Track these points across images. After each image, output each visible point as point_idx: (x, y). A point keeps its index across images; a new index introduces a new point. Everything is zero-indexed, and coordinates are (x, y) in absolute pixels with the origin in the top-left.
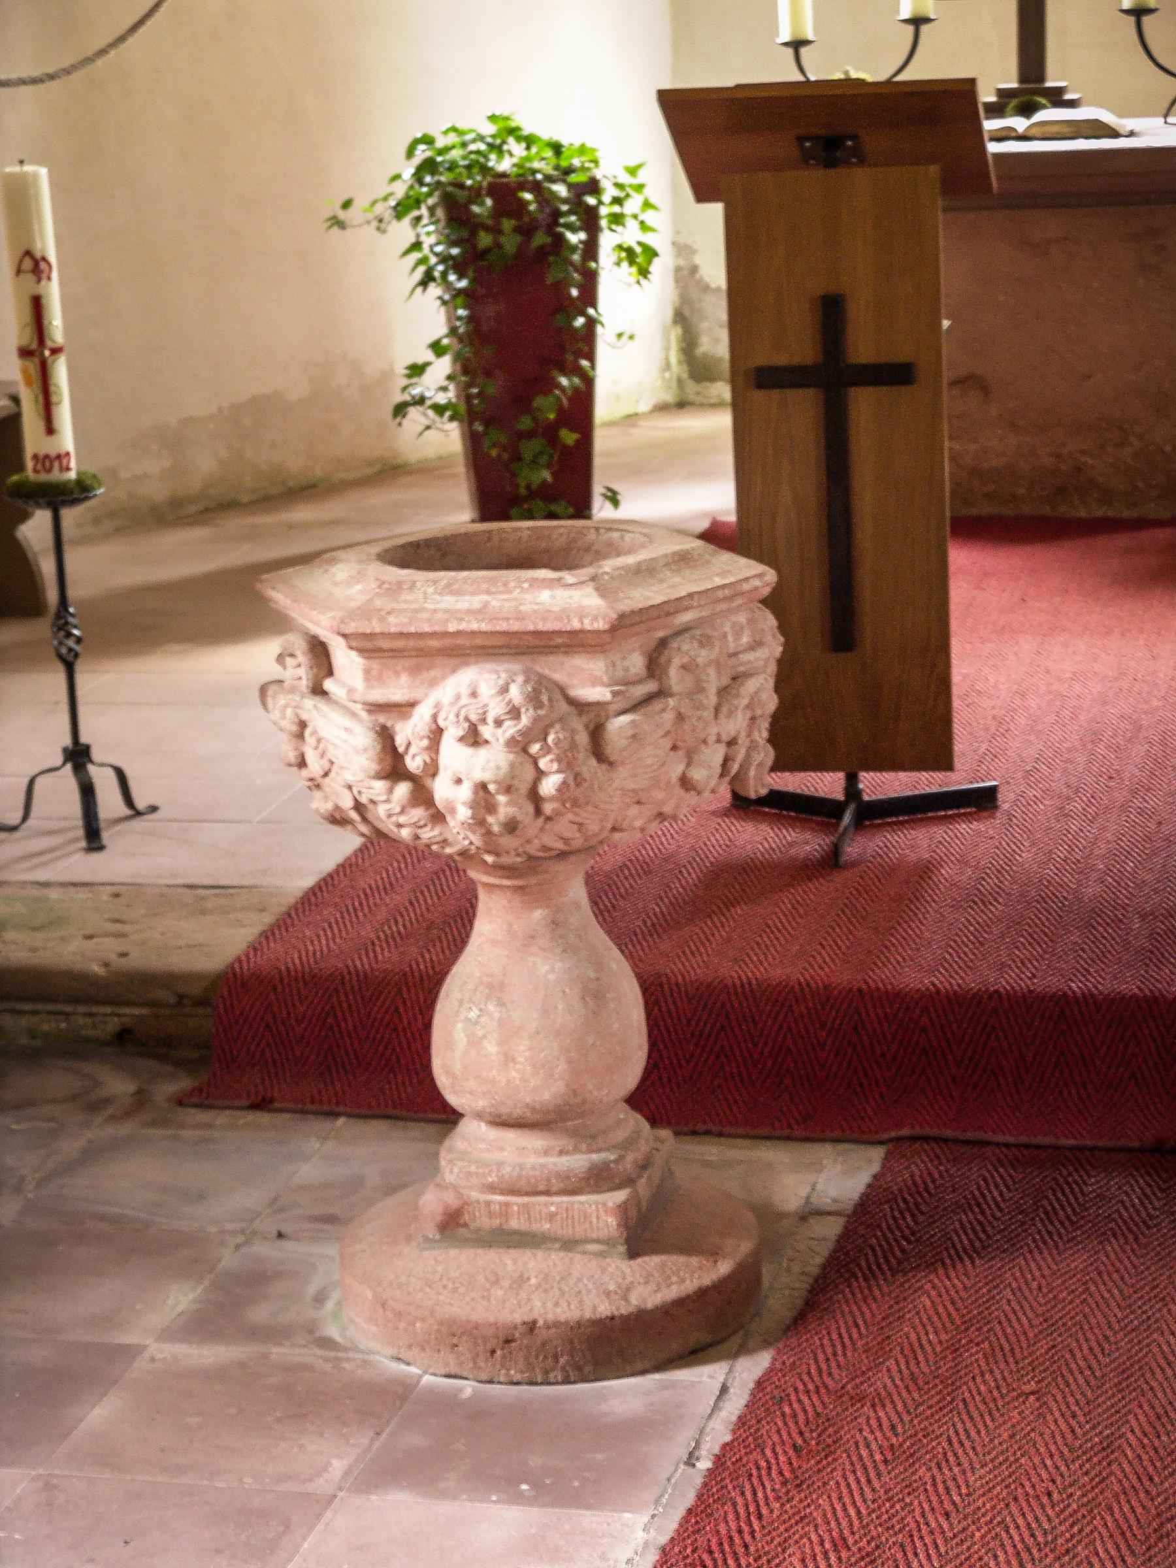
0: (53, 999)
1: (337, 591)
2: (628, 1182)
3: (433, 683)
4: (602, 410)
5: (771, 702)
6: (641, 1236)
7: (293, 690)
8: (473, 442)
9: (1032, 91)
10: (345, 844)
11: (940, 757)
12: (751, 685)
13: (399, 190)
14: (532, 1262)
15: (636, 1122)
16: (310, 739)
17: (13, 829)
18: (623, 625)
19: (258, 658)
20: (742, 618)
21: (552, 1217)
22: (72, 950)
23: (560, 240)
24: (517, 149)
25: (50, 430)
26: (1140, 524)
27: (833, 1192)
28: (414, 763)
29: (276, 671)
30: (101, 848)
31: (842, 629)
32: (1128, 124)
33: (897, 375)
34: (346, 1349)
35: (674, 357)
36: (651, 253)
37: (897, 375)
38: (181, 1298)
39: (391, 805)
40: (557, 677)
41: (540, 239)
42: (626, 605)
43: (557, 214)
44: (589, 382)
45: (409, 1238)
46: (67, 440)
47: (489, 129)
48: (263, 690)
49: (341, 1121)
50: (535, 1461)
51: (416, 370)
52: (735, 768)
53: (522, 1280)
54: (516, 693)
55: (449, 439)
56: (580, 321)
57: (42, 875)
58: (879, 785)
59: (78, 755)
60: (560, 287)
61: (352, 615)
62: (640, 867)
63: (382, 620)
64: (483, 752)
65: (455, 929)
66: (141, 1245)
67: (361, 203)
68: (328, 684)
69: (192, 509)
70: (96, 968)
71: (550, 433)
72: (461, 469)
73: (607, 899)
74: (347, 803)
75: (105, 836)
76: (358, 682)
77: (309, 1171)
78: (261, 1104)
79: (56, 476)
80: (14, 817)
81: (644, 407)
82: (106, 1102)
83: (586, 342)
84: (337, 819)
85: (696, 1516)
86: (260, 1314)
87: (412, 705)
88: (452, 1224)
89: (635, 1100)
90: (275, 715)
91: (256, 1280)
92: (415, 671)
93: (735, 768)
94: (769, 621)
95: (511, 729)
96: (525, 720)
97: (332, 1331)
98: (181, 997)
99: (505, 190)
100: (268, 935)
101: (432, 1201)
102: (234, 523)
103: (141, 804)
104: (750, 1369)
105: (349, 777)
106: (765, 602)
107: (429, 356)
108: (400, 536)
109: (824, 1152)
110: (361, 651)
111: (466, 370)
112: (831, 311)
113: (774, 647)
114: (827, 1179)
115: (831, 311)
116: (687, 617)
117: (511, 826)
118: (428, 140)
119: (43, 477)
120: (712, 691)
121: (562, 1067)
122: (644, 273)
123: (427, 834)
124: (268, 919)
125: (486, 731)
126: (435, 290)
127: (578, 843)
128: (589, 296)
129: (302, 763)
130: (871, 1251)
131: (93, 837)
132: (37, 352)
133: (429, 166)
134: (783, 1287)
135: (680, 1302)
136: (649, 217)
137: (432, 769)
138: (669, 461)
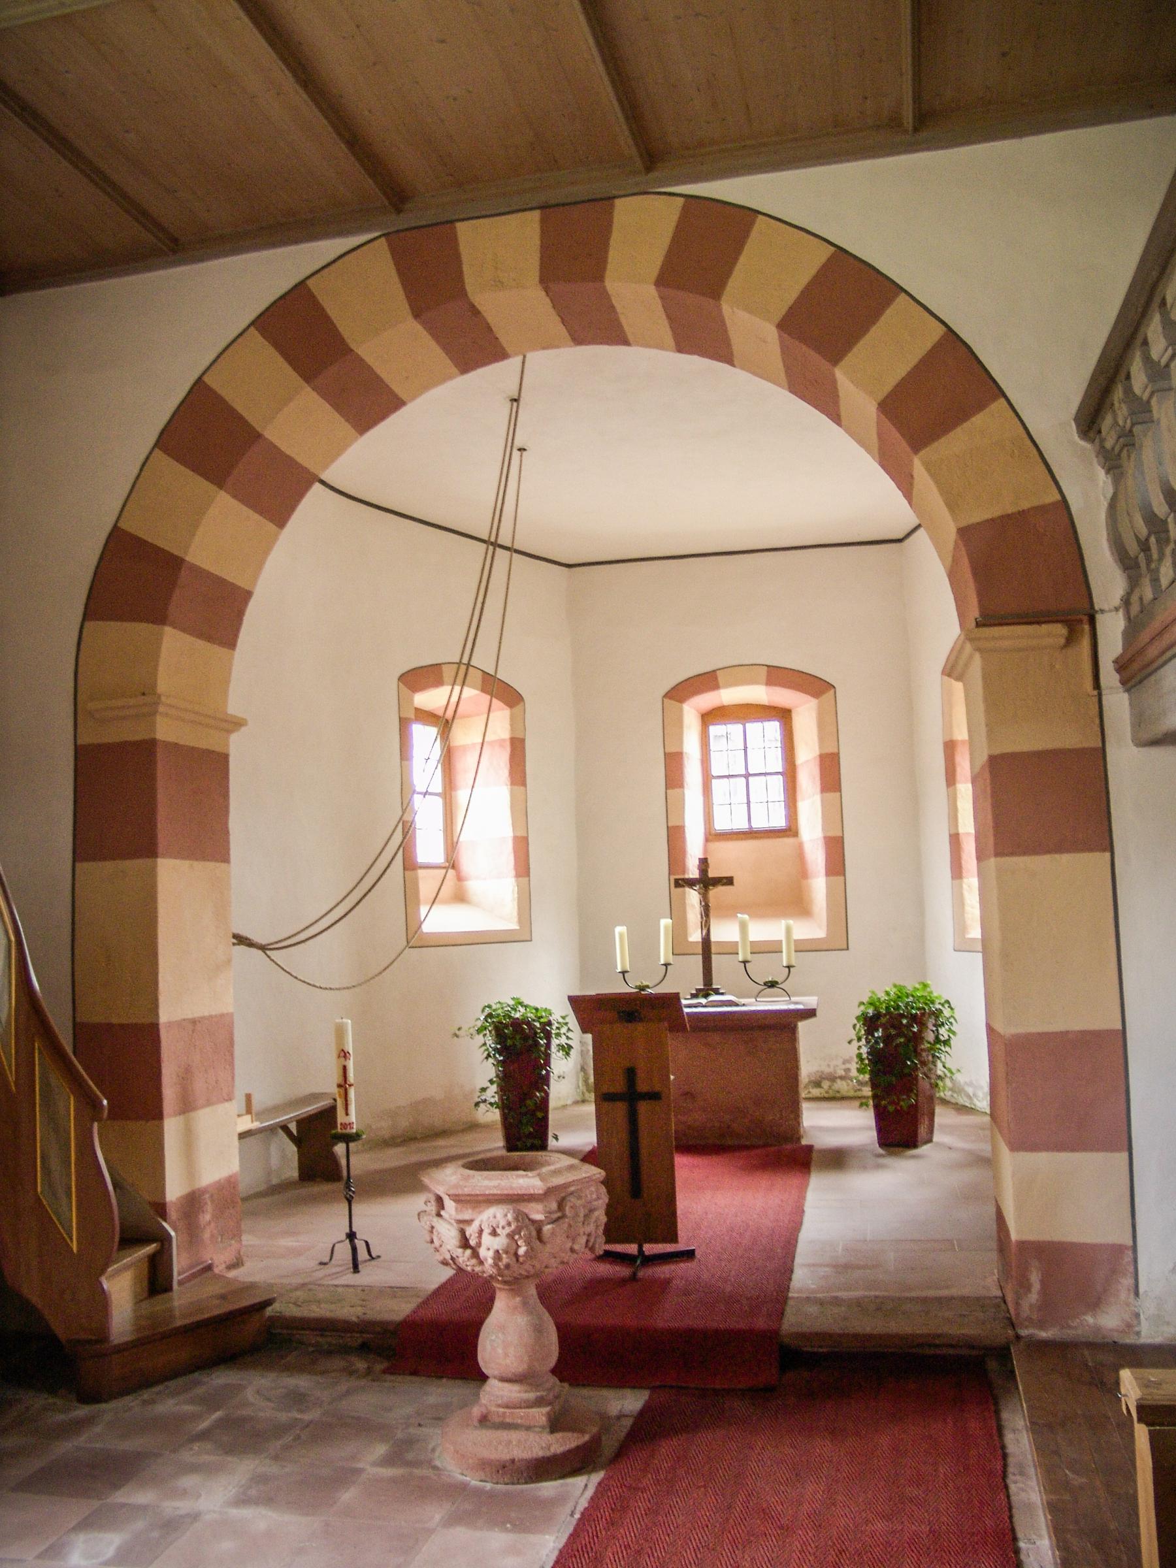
0: (337, 1331)
2: (550, 1404)
3: (480, 1212)
4: (552, 1104)
5: (604, 1219)
6: (555, 1425)
8: (505, 1117)
9: (707, 989)
10: (448, 1273)
11: (673, 1237)
12: (596, 1213)
13: (479, 1024)
14: (514, 1436)
15: (554, 1380)
17: (325, 1264)
18: (549, 1192)
19: (418, 1202)
20: (593, 1189)
21: (522, 1418)
22: (348, 1312)
24: (522, 1010)
25: (347, 1114)
26: (753, 1147)
27: (631, 1408)
28: (472, 1242)
29: (424, 1208)
31: (636, 1190)
32: (743, 1001)
33: (654, 1096)
36: (570, 1047)
37: (654, 1096)
38: (381, 1449)
39: (463, 1257)
40: (526, 1211)
42: (550, 1185)
43: (536, 1033)
44: (547, 1094)
45: (468, 1425)
46: (353, 1118)
47: (512, 1003)
48: (419, 1215)
50: (513, 1515)
51: (484, 1090)
52: (590, 1244)
53: (510, 1442)
54: (510, 1217)
55: (495, 1115)
56: (544, 1072)
57: (336, 1282)
58: (650, 1249)
59: (351, 1236)
60: (537, 1059)
62: (558, 1281)
64: (497, 1239)
65: (486, 1305)
66: (365, 1428)
67: (465, 1028)
68: (442, 1213)
70: (354, 1319)
71: (533, 1113)
72: (499, 1126)
73: (545, 1295)
74: (448, 1257)
75: (360, 1267)
76: (453, 1212)
77: (432, 1400)
78: (415, 1373)
79: (348, 1131)
80: (326, 1260)
81: (569, 1102)
82: (356, 1371)
83: (546, 1080)
84: (445, 1263)
85: (574, 1536)
86: (410, 1456)
87: (472, 1221)
88: (484, 1421)
89: (554, 1371)
90: (423, 1223)
91: (410, 1442)
92: (474, 1208)
93: (590, 1244)
94: (603, 1190)
95: (508, 1230)
96: (513, 1227)
97: (438, 1463)
99: (517, 1024)
101: (476, 1411)
102: (414, 1146)
104: (597, 1477)
105: (449, 1247)
106: (602, 1182)
107: (489, 1084)
108: (478, 1153)
109: (628, 1392)
111: (502, 1090)
112: (631, 1073)
113: (605, 1199)
114: (627, 1403)
115: (631, 1073)
116: (572, 1189)
117: (507, 1266)
118: (489, 1006)
120: (582, 1215)
121: (526, 1359)
122: (568, 1054)
123: (477, 1269)
124: (420, 1300)
125: (499, 1231)
126: (491, 1060)
127: (532, 1271)
128: (548, 1063)
129: (432, 1242)
130: (645, 1431)
131: (356, 1268)
132: (344, 1085)
133: (490, 1015)
134: (609, 1445)
135: (570, 1451)
136: (570, 1034)
137: (479, 1244)
138: (575, 1125)
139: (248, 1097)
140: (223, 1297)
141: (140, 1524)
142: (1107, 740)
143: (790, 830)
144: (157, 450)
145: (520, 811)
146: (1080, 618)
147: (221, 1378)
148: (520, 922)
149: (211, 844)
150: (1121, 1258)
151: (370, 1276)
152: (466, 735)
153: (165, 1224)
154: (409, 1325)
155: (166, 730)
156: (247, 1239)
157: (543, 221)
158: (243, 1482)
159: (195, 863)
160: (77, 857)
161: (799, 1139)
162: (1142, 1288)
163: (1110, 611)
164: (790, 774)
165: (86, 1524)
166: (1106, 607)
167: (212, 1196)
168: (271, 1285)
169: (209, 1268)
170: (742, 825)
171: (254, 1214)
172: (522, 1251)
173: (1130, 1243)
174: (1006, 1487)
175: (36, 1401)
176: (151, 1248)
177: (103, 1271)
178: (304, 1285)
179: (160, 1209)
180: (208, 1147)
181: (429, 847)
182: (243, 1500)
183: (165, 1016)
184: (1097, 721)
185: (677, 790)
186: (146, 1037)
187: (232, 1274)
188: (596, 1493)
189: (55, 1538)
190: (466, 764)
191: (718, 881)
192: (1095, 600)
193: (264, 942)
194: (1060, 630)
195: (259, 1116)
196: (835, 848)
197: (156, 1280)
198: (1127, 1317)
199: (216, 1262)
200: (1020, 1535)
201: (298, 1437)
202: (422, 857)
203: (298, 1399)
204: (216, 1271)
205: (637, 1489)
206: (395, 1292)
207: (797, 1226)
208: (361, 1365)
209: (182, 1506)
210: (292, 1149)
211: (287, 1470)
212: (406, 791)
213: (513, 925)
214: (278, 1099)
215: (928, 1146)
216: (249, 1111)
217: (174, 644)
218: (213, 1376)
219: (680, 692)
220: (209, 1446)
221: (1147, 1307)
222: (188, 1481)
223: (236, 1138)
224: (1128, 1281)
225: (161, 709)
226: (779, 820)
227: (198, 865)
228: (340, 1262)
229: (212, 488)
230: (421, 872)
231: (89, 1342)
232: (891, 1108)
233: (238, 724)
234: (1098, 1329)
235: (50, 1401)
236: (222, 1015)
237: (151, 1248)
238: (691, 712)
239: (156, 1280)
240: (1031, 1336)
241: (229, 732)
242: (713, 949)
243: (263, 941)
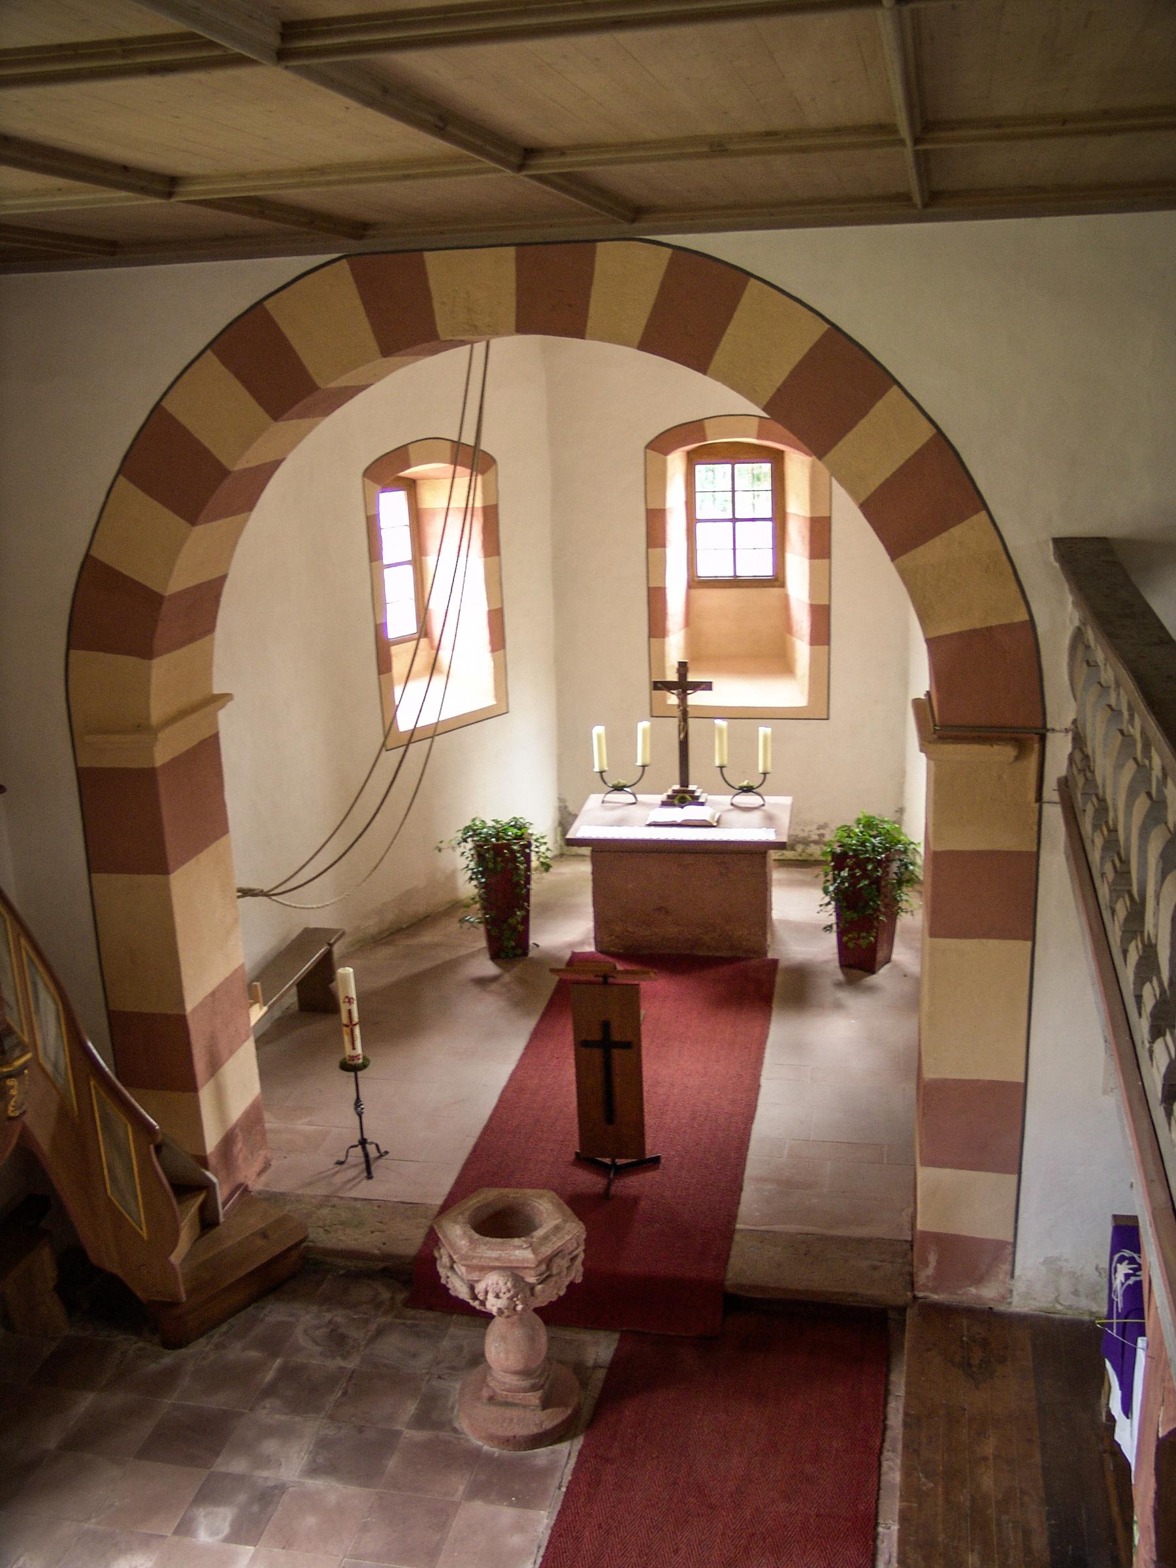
2: (542, 1387)
6: (546, 1404)
23: (517, 868)
25: (354, 1049)
35: (559, 838)
41: (510, 865)
49: (454, 1317)
50: (516, 1487)
53: (511, 1420)
54: (509, 1285)
56: (524, 891)
66: (397, 1380)
70: (376, 1251)
77: (446, 1343)
80: (342, 1159)
88: (491, 1399)
95: (508, 1295)
103: (382, 1151)
104: (578, 1443)
112: (606, 1026)
126: (474, 883)
140: (264, 1234)
141: (242, 1498)
142: (1042, 845)
143: (777, 580)
145: (495, 583)
146: (1029, 735)
148: (497, 697)
150: (1003, 1252)
151: (380, 1188)
152: (433, 499)
153: (208, 1174)
157: (519, 260)
160: (90, 870)
161: (765, 954)
162: (1017, 1273)
163: (1060, 731)
164: (779, 517)
166: (1057, 727)
170: (728, 572)
172: (519, 1307)
173: (1011, 1240)
174: (880, 1465)
179: (203, 1161)
181: (400, 621)
182: (314, 1470)
184: (1035, 828)
185: (659, 550)
188: (577, 1463)
190: (433, 529)
191: (697, 686)
192: (1049, 719)
194: (1009, 752)
196: (821, 615)
197: (207, 1221)
198: (1002, 1291)
200: (881, 1521)
201: (345, 1393)
202: (392, 633)
205: (607, 1460)
207: (750, 1118)
213: (492, 702)
215: (887, 966)
219: (662, 444)
221: (1019, 1286)
222: (270, 1446)
224: (1006, 1267)
226: (765, 569)
232: (851, 945)
233: (226, 697)
234: (979, 1298)
237: (201, 1198)
238: (676, 462)
240: (925, 1298)
242: (691, 713)
243: (357, 1118)
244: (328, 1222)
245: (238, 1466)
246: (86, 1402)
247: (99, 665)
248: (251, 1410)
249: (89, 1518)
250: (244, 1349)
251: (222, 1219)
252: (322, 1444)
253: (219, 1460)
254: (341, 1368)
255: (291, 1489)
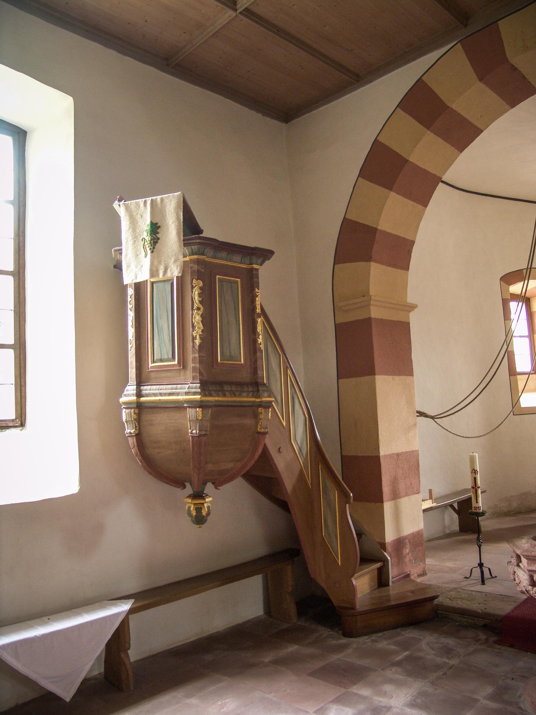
1: (522, 545)
7: (513, 565)
16: (516, 576)
17: (468, 578)
22: (475, 606)
25: (477, 502)
30: (484, 584)
34: (524, 711)
38: (489, 690)
46: (480, 504)
49: (529, 653)
57: (472, 589)
59: (481, 565)
61: (525, 551)
63: (531, 553)
68: (520, 564)
69: (512, 513)
74: (524, 590)
76: (526, 565)
77: (521, 664)
78: (512, 646)
79: (478, 511)
82: (479, 640)
98: (496, 620)
100: (515, 608)
103: (493, 576)
110: (526, 559)
119: (475, 511)
124: (516, 604)
129: (515, 580)
131: (483, 582)
132: (475, 487)
139: (430, 491)
140: (413, 592)
141: (362, 707)
144: (360, 178)
147: (409, 634)
149: (403, 366)
151: (489, 588)
153: (385, 553)
154: (508, 619)
155: (375, 313)
156: (428, 561)
158: (415, 694)
159: (395, 377)
160: (338, 377)
165: (337, 700)
167: (409, 541)
168: (439, 587)
169: (408, 576)
171: (436, 549)
175: (324, 631)
176: (379, 565)
177: (352, 576)
178: (455, 589)
179: (383, 546)
180: (406, 516)
182: (413, 705)
183: (383, 452)
186: (374, 462)
187: (419, 580)
189: (323, 704)
193: (433, 415)
195: (436, 500)
197: (382, 580)
199: (412, 573)
201: (445, 674)
202: (519, 368)
203: (448, 651)
204: (412, 577)
206: (503, 598)
208: (482, 636)
209: (382, 701)
210: (456, 516)
211: (438, 691)
212: (508, 335)
214: (448, 492)
216: (431, 498)
217: (376, 270)
218: (407, 632)
220: (400, 669)
222: (388, 688)
223: (422, 511)
225: (372, 302)
227: (397, 378)
228: (476, 578)
229: (387, 191)
230: (519, 377)
231: (348, 608)
233: (413, 307)
235: (331, 633)
236: (413, 451)
237: (379, 565)
239: (382, 580)
241: (410, 311)
243: (433, 414)
244: (453, 597)
245: (366, 692)
246: (292, 648)
247: (348, 383)
248: (382, 669)
249: (271, 693)
250: (388, 644)
251: (391, 584)
252: (422, 694)
253: (355, 687)
254: (445, 662)
255: (394, 710)
